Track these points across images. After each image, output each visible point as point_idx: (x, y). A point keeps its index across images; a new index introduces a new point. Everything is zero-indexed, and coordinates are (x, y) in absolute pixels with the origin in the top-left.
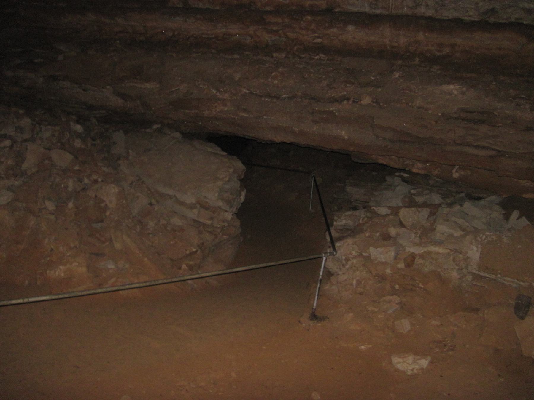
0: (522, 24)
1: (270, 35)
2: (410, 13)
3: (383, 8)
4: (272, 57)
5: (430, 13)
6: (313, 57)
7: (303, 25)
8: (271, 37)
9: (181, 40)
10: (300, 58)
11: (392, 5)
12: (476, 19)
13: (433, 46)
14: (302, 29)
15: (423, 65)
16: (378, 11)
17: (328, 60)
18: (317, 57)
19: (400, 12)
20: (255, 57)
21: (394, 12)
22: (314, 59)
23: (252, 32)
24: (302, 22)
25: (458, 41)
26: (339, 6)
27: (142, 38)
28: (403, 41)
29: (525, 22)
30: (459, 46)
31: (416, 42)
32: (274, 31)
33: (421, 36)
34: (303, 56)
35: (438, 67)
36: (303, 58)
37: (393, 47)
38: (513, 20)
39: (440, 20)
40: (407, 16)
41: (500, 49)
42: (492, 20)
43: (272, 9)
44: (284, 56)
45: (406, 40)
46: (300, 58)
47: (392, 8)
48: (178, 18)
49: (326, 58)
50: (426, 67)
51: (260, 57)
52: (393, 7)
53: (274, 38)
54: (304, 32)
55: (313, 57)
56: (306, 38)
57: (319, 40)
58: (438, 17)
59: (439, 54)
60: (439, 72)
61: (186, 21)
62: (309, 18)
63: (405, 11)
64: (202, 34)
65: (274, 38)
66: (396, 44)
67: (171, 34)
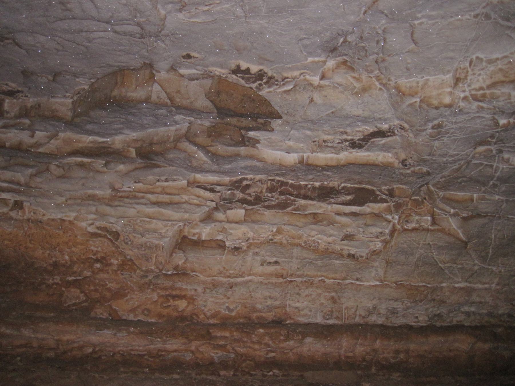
0: (464, 326)
1: (216, 351)
2: (362, 322)
3: (337, 318)
4: (219, 375)
5: (380, 321)
6: (266, 373)
7: (255, 339)
8: (217, 353)
9: (103, 358)
10: (251, 375)
11: (345, 314)
12: (425, 325)
13: (389, 353)
14: (253, 342)
15: (381, 373)
16: (331, 322)
17: (282, 376)
18: (271, 373)
19: (352, 322)
20: (198, 376)
21: (347, 322)
22: (267, 375)
23: (193, 348)
24: (253, 336)
25: (412, 346)
26: (291, 318)
27: (52, 354)
28: (360, 350)
29: (466, 324)
30: (413, 351)
31: (374, 350)
32: (221, 346)
33: (378, 344)
34: (254, 373)
35: (398, 374)
36: (255, 374)
37: (348, 357)
38: (455, 323)
39: (394, 328)
40: (361, 325)
41: (450, 351)
42: (438, 324)
43: (218, 322)
44: (232, 373)
45: (362, 349)
46: (251, 375)
47: (345, 318)
48: (106, 331)
49: (281, 374)
50: (384, 375)
51: (204, 376)
52: (346, 317)
53: (220, 353)
54: (256, 346)
55: (266, 373)
56: (258, 353)
57: (272, 355)
58: (389, 324)
59: (393, 361)
60: (399, 379)
61: (115, 335)
62: (261, 331)
63: (357, 320)
64: (132, 350)
65: (220, 353)
66: (351, 354)
67: (90, 350)
